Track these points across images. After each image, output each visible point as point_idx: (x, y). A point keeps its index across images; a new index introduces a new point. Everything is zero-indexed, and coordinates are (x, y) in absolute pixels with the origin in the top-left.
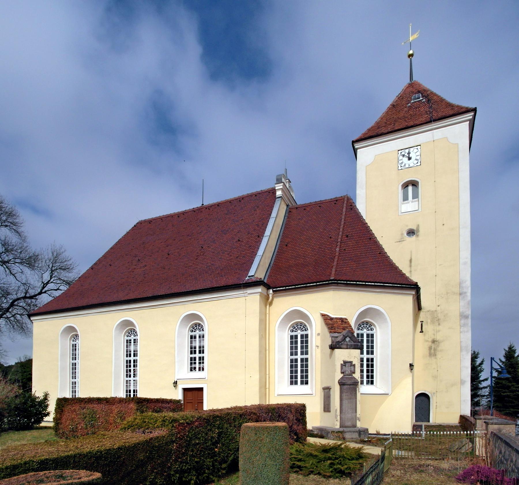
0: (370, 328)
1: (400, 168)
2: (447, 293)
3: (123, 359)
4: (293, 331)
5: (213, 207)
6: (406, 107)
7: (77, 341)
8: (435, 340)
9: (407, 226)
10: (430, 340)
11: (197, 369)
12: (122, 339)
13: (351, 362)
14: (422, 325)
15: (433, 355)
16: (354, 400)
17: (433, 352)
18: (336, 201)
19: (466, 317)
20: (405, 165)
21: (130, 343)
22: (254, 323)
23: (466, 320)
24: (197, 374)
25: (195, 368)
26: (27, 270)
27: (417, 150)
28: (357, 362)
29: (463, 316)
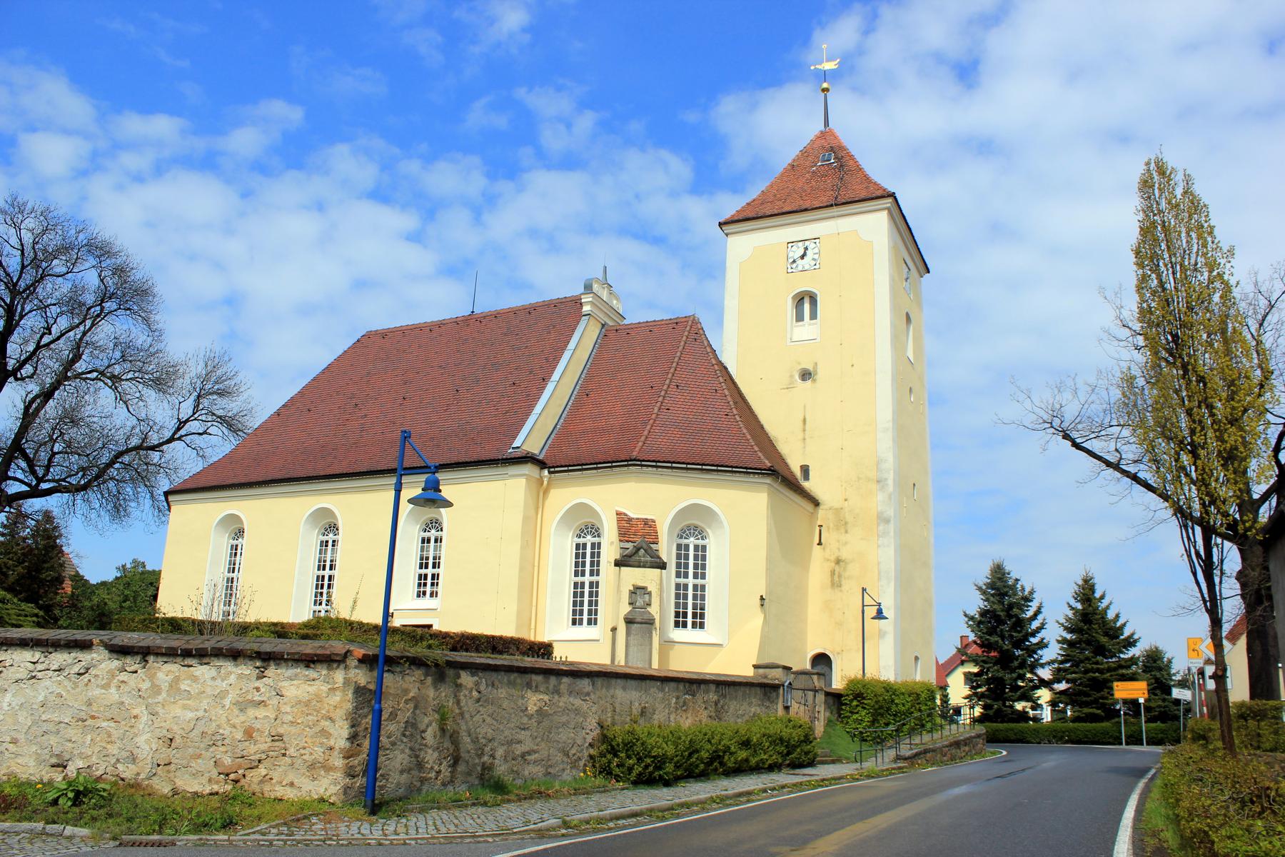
1: (790, 270)
2: (859, 479)
3: (312, 572)
4: (579, 536)
5: (487, 319)
6: (809, 172)
7: (240, 540)
10: (833, 558)
11: (585, 621)
12: (315, 538)
13: (644, 588)
14: (820, 531)
16: (648, 647)
18: (676, 323)
19: (887, 521)
21: (326, 546)
22: (514, 522)
24: (427, 602)
25: (424, 593)
26: (150, 394)
27: (814, 245)
28: (652, 588)
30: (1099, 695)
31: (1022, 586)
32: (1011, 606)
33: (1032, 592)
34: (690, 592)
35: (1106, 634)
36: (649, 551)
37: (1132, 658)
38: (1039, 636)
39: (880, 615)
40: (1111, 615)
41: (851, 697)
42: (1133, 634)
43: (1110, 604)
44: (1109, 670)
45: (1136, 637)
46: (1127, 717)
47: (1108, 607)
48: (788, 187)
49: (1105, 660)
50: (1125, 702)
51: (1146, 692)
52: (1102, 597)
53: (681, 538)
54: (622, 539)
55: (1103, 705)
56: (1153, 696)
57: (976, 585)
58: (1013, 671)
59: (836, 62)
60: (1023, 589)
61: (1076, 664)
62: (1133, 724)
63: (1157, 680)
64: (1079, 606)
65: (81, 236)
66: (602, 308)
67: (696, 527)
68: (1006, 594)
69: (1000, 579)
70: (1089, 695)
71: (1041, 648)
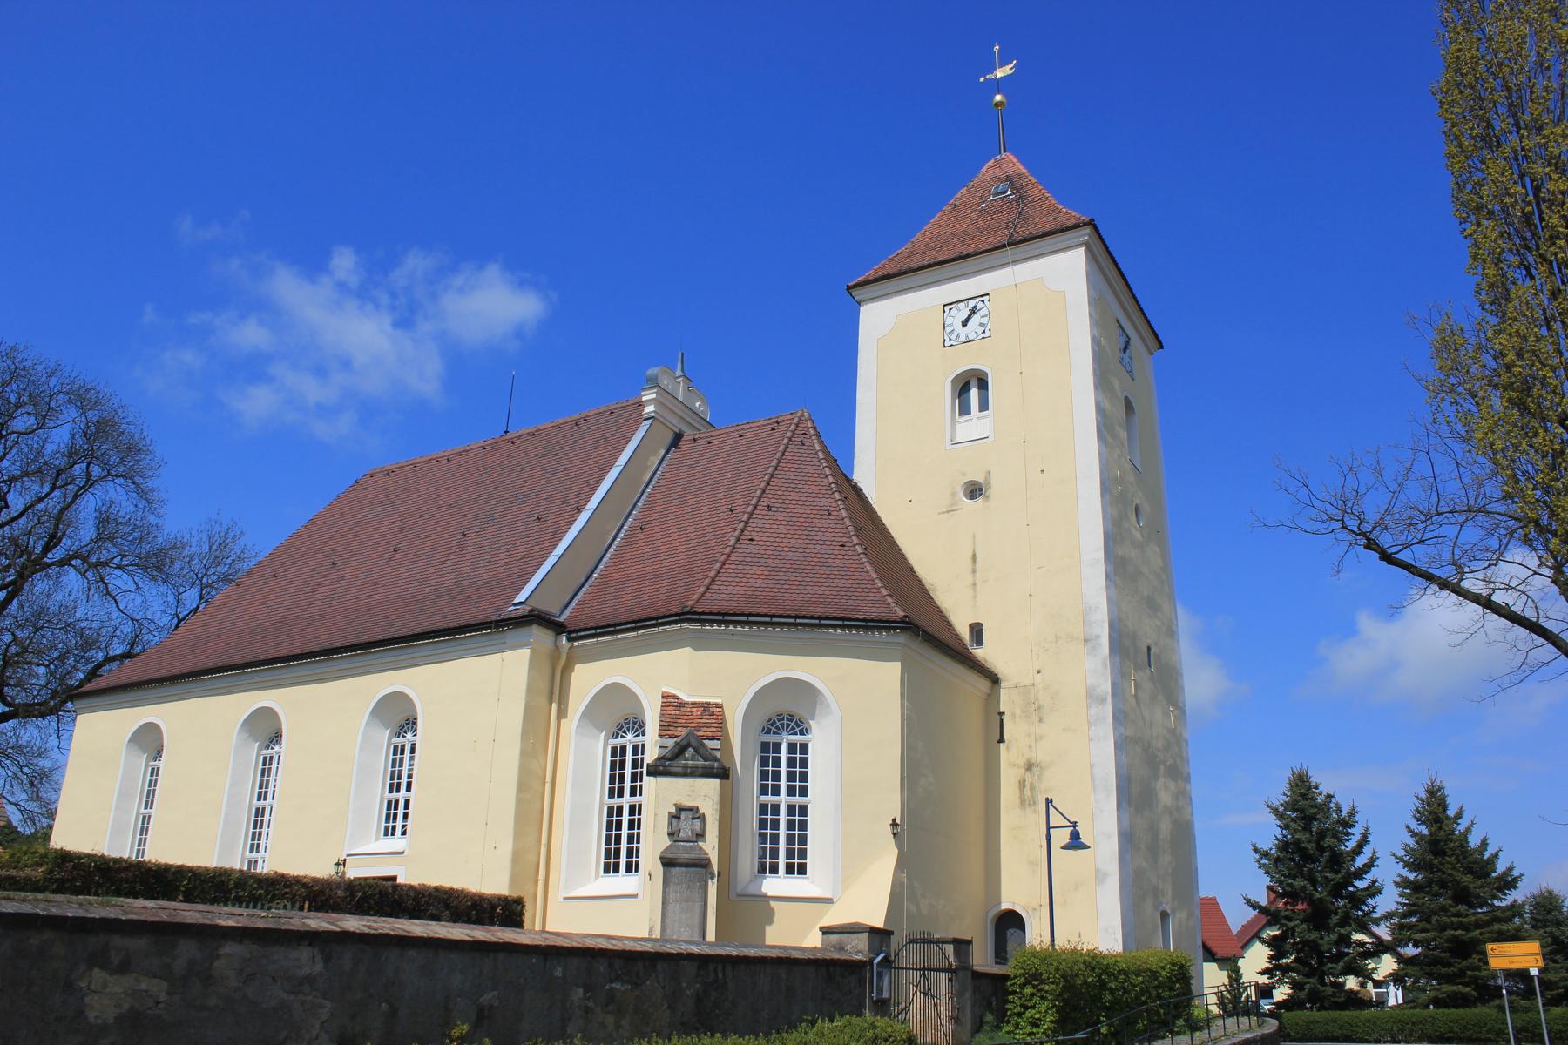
0: (636, 726)
1: (948, 343)
5: (523, 438)
6: (975, 211)
8: (1033, 761)
9: (964, 474)
10: (1022, 762)
13: (693, 810)
15: (1030, 804)
17: (1029, 794)
19: (1102, 700)
20: (958, 336)
23: (1100, 707)
24: (397, 843)
29: (1093, 697)
30: (1464, 963)
31: (1337, 805)
32: (1322, 834)
33: (1352, 813)
34: (783, 817)
35: (1469, 871)
36: (702, 750)
37: (1513, 906)
38: (1369, 877)
39: (1075, 843)
40: (1474, 841)
41: (1023, 980)
42: (1510, 869)
43: (1472, 825)
44: (1478, 925)
45: (1515, 873)
46: (1514, 997)
47: (1468, 831)
48: (945, 233)
49: (1471, 911)
50: (1510, 974)
51: (1539, 958)
52: (1459, 815)
53: (768, 732)
54: (664, 732)
55: (1476, 978)
56: (1551, 964)
57: (1269, 807)
58: (1330, 930)
59: (1012, 65)
60: (1339, 810)
61: (1426, 918)
62: (1527, 1010)
63: (1556, 940)
64: (1425, 831)
65: (53, 381)
66: (688, 419)
67: (791, 717)
68: (1313, 818)
69: (1303, 795)
70: (1449, 965)
71: (1373, 896)
